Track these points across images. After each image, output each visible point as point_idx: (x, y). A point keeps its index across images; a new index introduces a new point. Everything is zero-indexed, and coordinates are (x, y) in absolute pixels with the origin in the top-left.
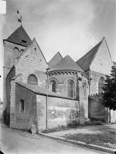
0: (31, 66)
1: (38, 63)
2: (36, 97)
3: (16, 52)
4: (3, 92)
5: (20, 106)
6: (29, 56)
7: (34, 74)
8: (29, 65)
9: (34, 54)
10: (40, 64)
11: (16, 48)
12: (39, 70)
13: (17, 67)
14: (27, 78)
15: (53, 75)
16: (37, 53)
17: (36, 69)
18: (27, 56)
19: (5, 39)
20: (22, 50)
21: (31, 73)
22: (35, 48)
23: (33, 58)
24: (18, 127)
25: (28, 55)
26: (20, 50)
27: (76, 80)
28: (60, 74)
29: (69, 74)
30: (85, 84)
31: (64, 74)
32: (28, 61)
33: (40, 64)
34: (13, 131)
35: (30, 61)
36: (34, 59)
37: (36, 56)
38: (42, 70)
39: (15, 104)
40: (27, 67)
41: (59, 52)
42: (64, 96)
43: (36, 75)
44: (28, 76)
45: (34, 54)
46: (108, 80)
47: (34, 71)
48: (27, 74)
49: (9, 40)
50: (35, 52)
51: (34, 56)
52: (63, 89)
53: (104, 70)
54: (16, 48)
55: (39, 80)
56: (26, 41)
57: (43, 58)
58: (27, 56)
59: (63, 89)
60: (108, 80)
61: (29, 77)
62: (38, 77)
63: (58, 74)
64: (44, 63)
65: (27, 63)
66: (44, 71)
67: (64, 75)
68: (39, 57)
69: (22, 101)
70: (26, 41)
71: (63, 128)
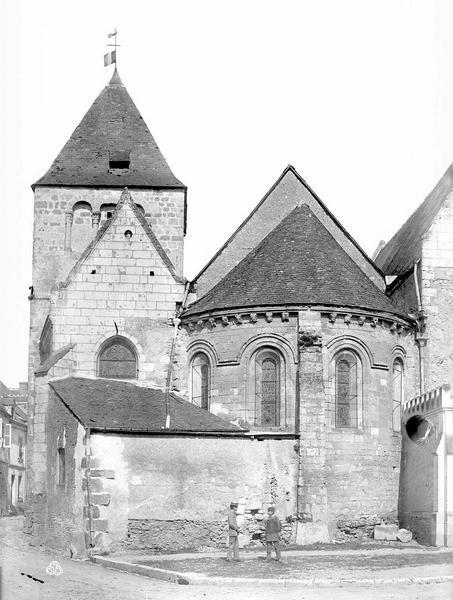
1: (141, 289)
3: (79, 221)
5: (58, 467)
6: (103, 270)
10: (148, 288)
11: (83, 204)
13: (57, 321)
15: (201, 328)
16: (134, 247)
17: (129, 313)
18: (94, 272)
19: (34, 182)
20: (104, 206)
22: (127, 229)
25: (99, 267)
26: (96, 209)
27: (294, 344)
28: (226, 325)
29: (262, 321)
30: (358, 355)
31: (239, 324)
33: (148, 288)
36: (125, 273)
37: (132, 262)
39: (45, 460)
41: (291, 169)
42: (203, 427)
44: (97, 348)
45: (121, 254)
49: (52, 181)
50: (128, 247)
52: (236, 391)
54: (83, 204)
55: (142, 358)
56: (111, 167)
57: (160, 262)
58: (94, 272)
59: (236, 391)
61: (101, 353)
63: (219, 326)
64: (165, 281)
65: (98, 296)
66: (164, 315)
67: (243, 326)
68: (146, 263)
69: (61, 451)
70: (111, 167)
71: (446, 508)
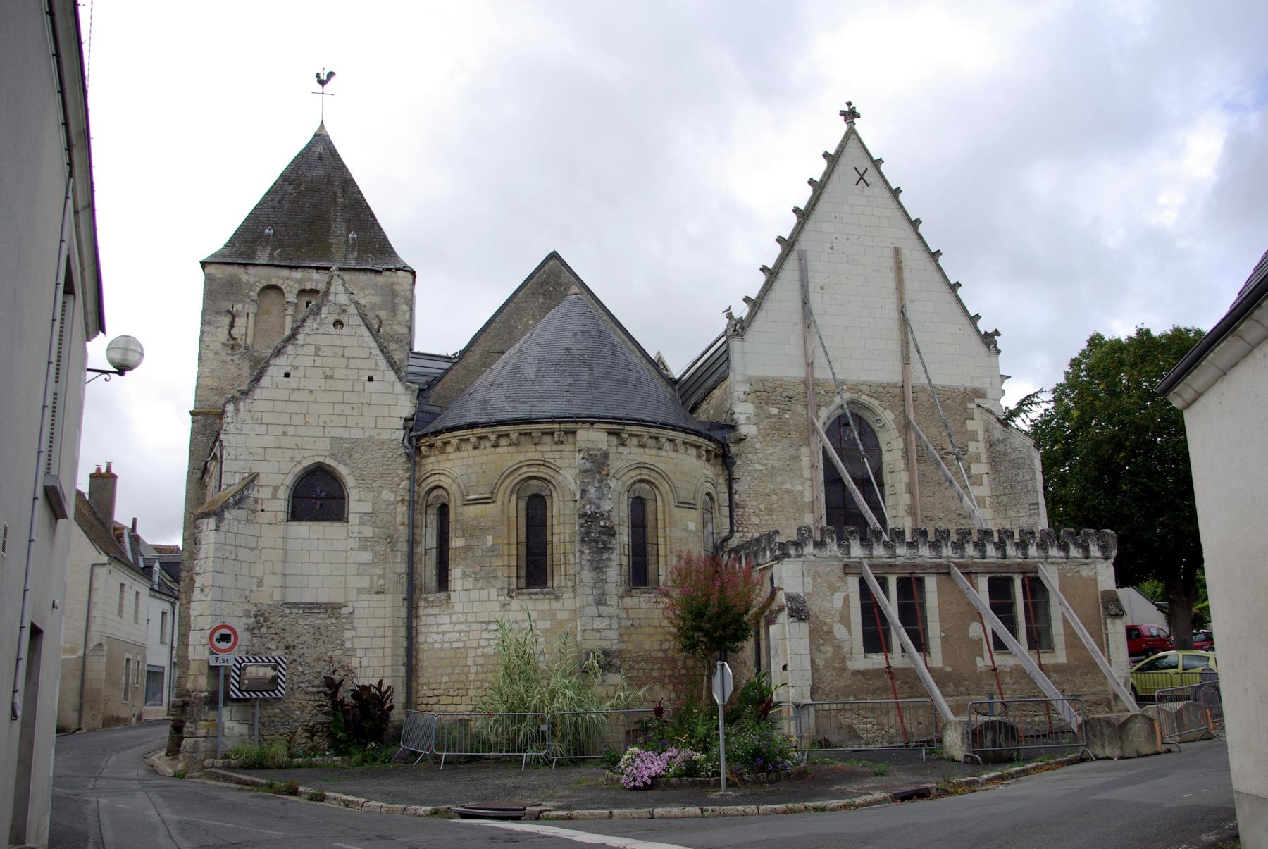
0: (310, 419)
1: (354, 399)
2: (1068, 658)
4: (1204, 587)
7: (329, 461)
8: (298, 420)
12: (356, 434)
14: (283, 494)
17: (338, 432)
21: (306, 463)
24: (635, 780)
32: (295, 396)
36: (332, 377)
38: (374, 433)
40: (285, 434)
46: (689, 561)
47: (326, 444)
48: (286, 467)
58: (287, 375)
60: (689, 561)
63: (668, 446)
67: (662, 453)
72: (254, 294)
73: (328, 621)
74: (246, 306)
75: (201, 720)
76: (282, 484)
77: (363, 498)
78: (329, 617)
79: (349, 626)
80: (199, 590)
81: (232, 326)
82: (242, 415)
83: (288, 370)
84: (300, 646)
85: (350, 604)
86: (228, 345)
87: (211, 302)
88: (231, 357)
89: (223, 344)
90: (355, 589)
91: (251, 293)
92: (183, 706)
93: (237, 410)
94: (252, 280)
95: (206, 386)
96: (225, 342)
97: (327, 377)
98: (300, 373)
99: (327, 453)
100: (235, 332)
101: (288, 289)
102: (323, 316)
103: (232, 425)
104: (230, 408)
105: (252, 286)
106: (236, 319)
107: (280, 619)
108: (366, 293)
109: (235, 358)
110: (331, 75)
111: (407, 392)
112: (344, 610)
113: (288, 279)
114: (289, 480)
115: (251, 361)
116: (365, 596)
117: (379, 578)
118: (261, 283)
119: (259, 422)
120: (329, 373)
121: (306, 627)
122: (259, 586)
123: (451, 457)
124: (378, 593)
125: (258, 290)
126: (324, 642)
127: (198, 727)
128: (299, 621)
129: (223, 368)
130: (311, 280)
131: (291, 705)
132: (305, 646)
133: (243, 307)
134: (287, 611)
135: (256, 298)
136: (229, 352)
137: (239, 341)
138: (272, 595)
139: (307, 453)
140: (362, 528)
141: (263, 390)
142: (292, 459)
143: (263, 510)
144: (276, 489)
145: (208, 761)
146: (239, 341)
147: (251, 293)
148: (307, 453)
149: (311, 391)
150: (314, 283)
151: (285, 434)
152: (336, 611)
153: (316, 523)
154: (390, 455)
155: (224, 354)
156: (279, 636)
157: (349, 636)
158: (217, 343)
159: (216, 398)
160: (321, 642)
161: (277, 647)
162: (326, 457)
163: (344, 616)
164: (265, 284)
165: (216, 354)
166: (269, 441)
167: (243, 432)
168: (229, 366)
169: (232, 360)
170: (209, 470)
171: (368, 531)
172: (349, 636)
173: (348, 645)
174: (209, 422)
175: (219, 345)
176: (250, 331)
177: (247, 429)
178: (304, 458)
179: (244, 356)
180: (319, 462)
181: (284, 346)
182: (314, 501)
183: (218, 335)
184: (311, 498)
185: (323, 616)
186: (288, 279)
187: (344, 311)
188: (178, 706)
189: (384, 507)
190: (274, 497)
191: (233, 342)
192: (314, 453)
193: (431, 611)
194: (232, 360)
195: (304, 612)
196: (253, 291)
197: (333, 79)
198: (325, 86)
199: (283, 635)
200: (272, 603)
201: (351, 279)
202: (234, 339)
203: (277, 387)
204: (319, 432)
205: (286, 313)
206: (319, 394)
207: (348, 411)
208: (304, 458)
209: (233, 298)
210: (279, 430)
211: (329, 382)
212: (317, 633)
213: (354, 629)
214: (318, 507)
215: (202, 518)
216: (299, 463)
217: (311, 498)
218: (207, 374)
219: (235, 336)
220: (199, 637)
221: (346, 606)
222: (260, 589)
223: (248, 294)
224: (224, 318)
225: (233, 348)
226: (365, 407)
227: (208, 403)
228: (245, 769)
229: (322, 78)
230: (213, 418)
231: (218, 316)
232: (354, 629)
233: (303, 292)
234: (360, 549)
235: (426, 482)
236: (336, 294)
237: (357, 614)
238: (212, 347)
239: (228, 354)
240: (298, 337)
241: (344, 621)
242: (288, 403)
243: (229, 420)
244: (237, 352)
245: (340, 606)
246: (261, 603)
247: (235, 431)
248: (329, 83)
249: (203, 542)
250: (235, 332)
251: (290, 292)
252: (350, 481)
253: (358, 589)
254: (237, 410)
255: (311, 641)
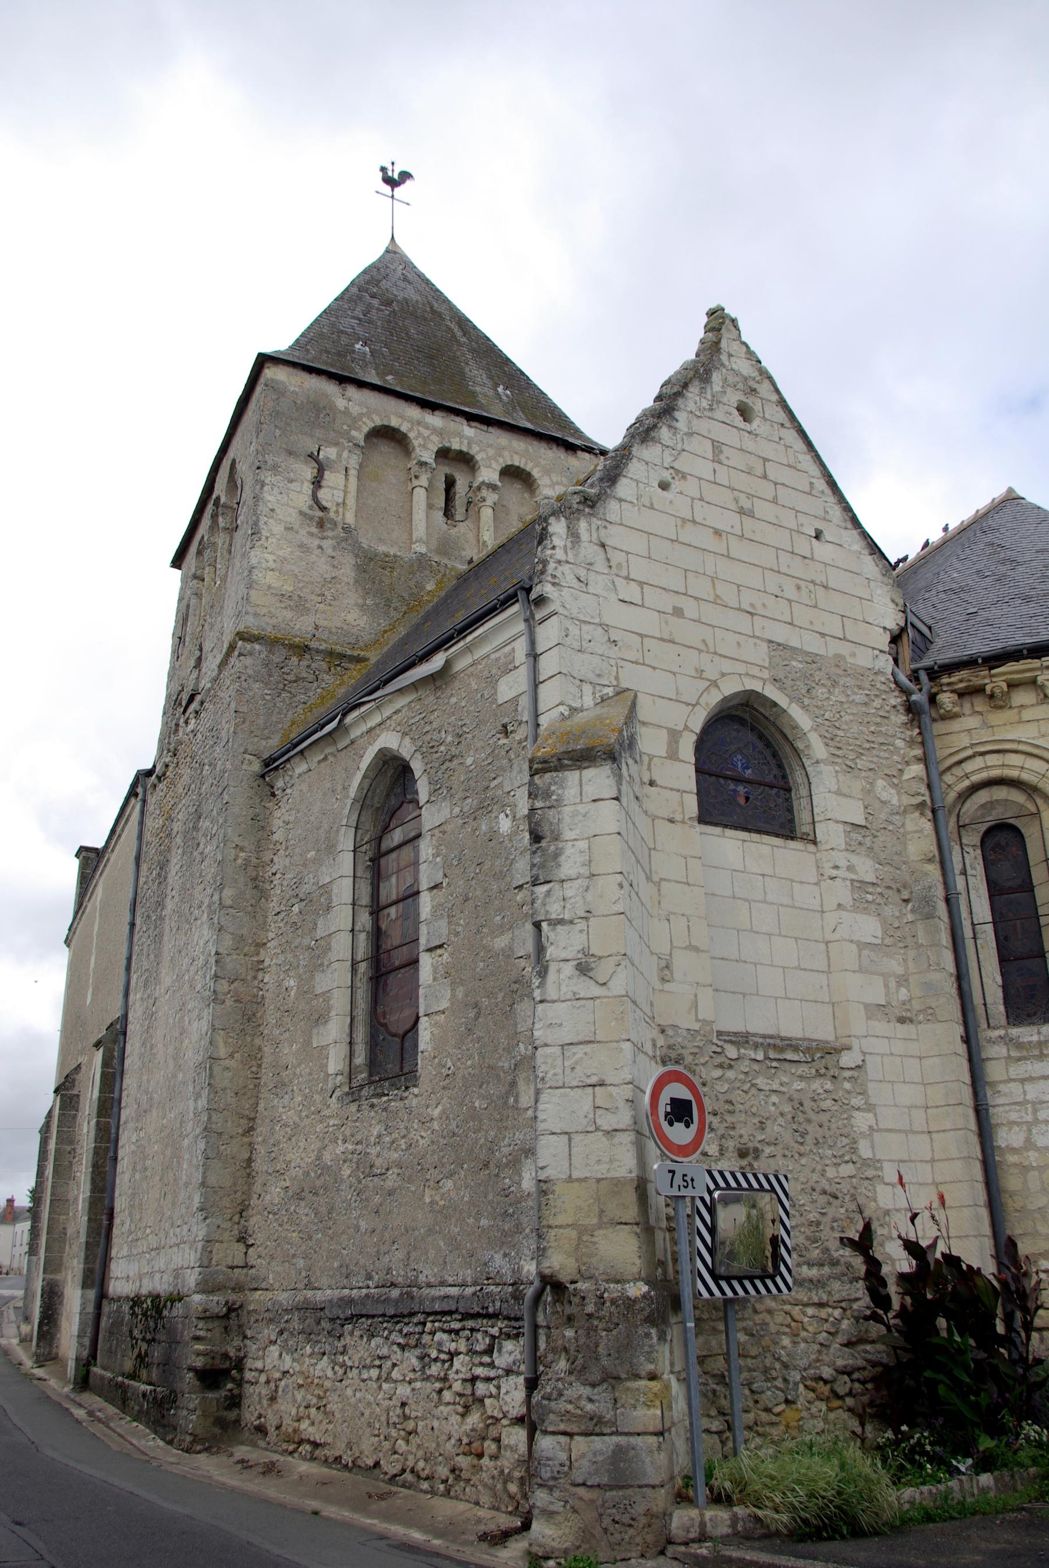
1: (797, 568)
7: (771, 692)
8: (700, 587)
9: (738, 460)
12: (813, 645)
17: (781, 634)
23: (742, 512)
32: (688, 534)
34: (438, 688)
35: (706, 540)
37: (767, 490)
38: (844, 649)
40: (678, 612)
43: (796, 712)
48: (691, 690)
51: (742, 481)
53: (780, 610)
62: (814, 739)
71: (347, 479)
72: (359, 436)
73: (816, 1085)
74: (345, 454)
75: (637, 1377)
76: (686, 727)
77: (845, 790)
78: (819, 1075)
79: (857, 1101)
80: (569, 969)
81: (317, 483)
82: (588, 550)
83: (667, 475)
84: (768, 1150)
85: (855, 1043)
86: (311, 518)
87: (278, 432)
88: (317, 542)
89: (301, 513)
90: (862, 1007)
91: (354, 433)
92: (226, 1316)
93: (574, 535)
94: (355, 410)
95: (269, 587)
96: (305, 509)
97: (742, 512)
98: (691, 487)
99: (766, 675)
100: (323, 495)
101: (420, 441)
102: (717, 388)
103: (566, 568)
104: (558, 528)
105: (355, 420)
106: (327, 474)
107: (718, 1073)
108: (554, 479)
109: (327, 544)
110: (405, 176)
111: (886, 580)
112: (847, 1059)
113: (419, 423)
114: (697, 723)
115: (357, 556)
116: (880, 1027)
117: (899, 985)
118: (372, 420)
119: (624, 573)
120: (746, 504)
121: (774, 1098)
122: (663, 980)
123: (1027, 715)
124: (902, 1020)
125: (366, 430)
126: (817, 1143)
127: (623, 1398)
128: (760, 1081)
129: (301, 559)
130: (461, 436)
131: (767, 1318)
132: (778, 1151)
133: (339, 455)
134: (732, 1052)
135: (362, 443)
136: (314, 530)
137: (332, 515)
138: (695, 1005)
139: (727, 666)
140: (855, 859)
141: (624, 505)
142: (700, 673)
143: (652, 783)
144: (674, 736)
145: (682, 1519)
146: (332, 515)
147: (354, 433)
148: (727, 666)
149: (718, 533)
150: (466, 442)
151: (678, 612)
152: (830, 1060)
153: (755, 836)
154: (877, 703)
155: (303, 532)
156: (723, 1120)
157: (864, 1128)
158: (291, 510)
159: (289, 614)
160: (809, 1139)
161: (722, 1151)
162: (764, 681)
163: (847, 1074)
164: (378, 421)
165: (287, 529)
166: (647, 621)
167: (591, 589)
168: (313, 558)
169: (320, 547)
170: (335, 742)
171: (866, 869)
172: (864, 1128)
173: (865, 1150)
174: (277, 658)
175: (294, 513)
176: (351, 501)
177: (598, 583)
178: (723, 675)
179: (343, 544)
180: (752, 692)
181: (655, 426)
182: (732, 786)
183: (293, 495)
184: (726, 778)
185: (802, 1069)
186: (419, 423)
187: (754, 390)
188: (218, 1317)
189: (883, 816)
190: (673, 755)
191: (321, 514)
192: (741, 668)
193: (1017, 1070)
194: (320, 547)
195: (767, 1058)
196: (358, 429)
197: (408, 183)
198: (396, 190)
199: (729, 1118)
200: (696, 1026)
201: (527, 450)
202: (323, 509)
203: (652, 507)
204: (743, 623)
205: (415, 483)
206: (733, 542)
207: (790, 592)
208: (723, 675)
209: (319, 433)
210: (667, 602)
211: (748, 522)
212: (801, 1118)
213: (870, 1108)
214: (741, 801)
215: (559, 767)
216: (714, 684)
217: (726, 778)
218: (271, 565)
219: (325, 503)
220: (587, 1106)
221: (849, 1048)
222: (667, 986)
223: (348, 432)
224: (304, 468)
225: (321, 524)
226: (820, 591)
227: (274, 621)
228: (803, 1538)
229: (390, 174)
230: (284, 652)
231: (291, 460)
232: (870, 1108)
233: (443, 454)
234: (855, 909)
235: (958, 771)
236: (730, 355)
237: (873, 1065)
238: (280, 513)
239: (311, 534)
240: (677, 414)
241: (847, 1085)
242: (676, 545)
243: (559, 554)
244: (330, 534)
245: (831, 1051)
246: (675, 1027)
247: (575, 583)
248: (402, 187)
249: (568, 835)
250: (323, 495)
251: (424, 447)
252: (817, 747)
253: (866, 1006)
254: (574, 535)
255: (788, 1137)
